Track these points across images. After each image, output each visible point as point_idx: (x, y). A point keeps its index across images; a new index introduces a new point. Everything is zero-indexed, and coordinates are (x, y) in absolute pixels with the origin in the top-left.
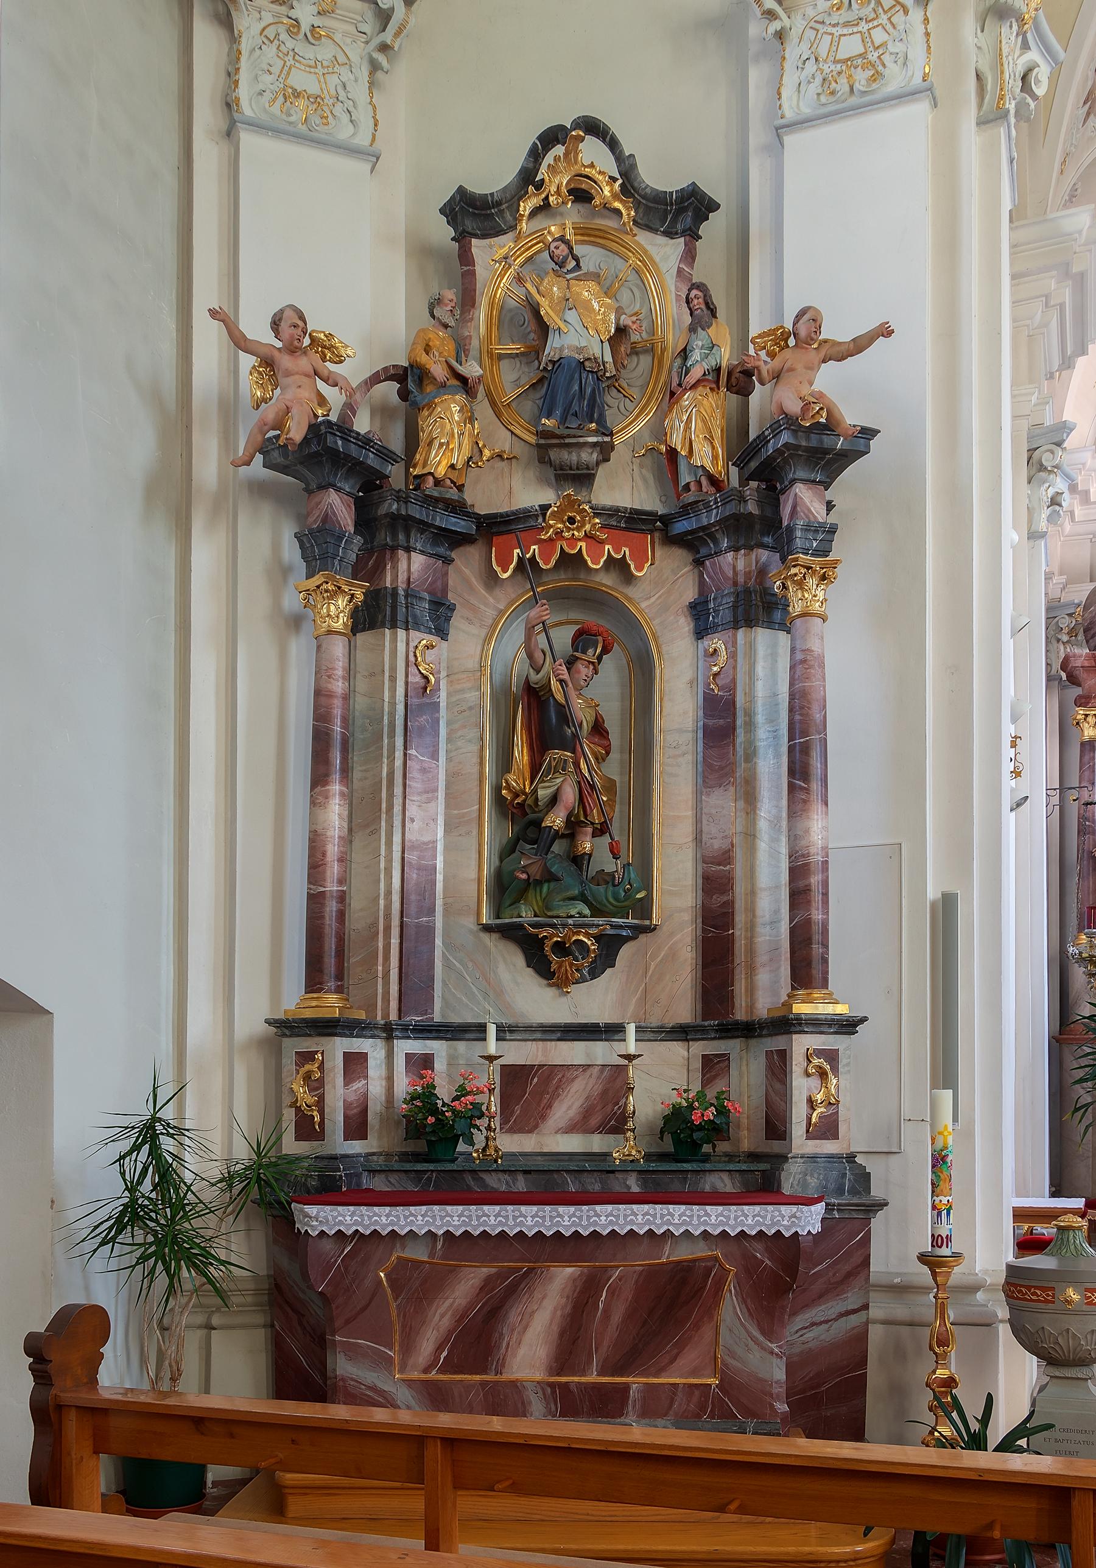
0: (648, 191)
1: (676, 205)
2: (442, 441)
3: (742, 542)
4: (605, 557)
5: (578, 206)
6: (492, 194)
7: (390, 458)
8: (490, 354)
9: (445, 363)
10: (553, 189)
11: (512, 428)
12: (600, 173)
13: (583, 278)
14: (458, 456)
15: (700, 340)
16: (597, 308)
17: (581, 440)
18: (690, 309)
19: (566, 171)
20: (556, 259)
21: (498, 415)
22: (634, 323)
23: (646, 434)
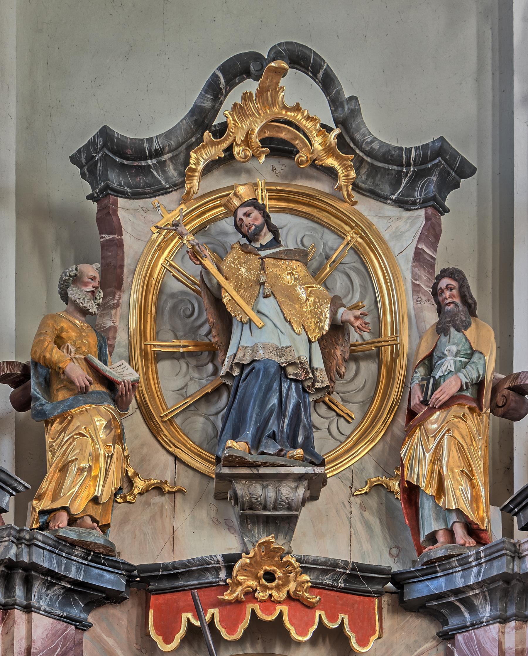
0: (376, 145)
1: (415, 165)
2: (83, 465)
3: (512, 610)
4: (315, 627)
5: (275, 162)
6: (150, 140)
7: (9, 486)
8: (145, 355)
9: (84, 362)
10: (240, 137)
11: (177, 452)
12: (309, 118)
13: (283, 256)
14: (104, 486)
15: (454, 344)
16: (304, 296)
17: (283, 470)
18: (438, 303)
19: (259, 114)
20: (245, 229)
21: (155, 432)
22: (357, 318)
23: (370, 467)
